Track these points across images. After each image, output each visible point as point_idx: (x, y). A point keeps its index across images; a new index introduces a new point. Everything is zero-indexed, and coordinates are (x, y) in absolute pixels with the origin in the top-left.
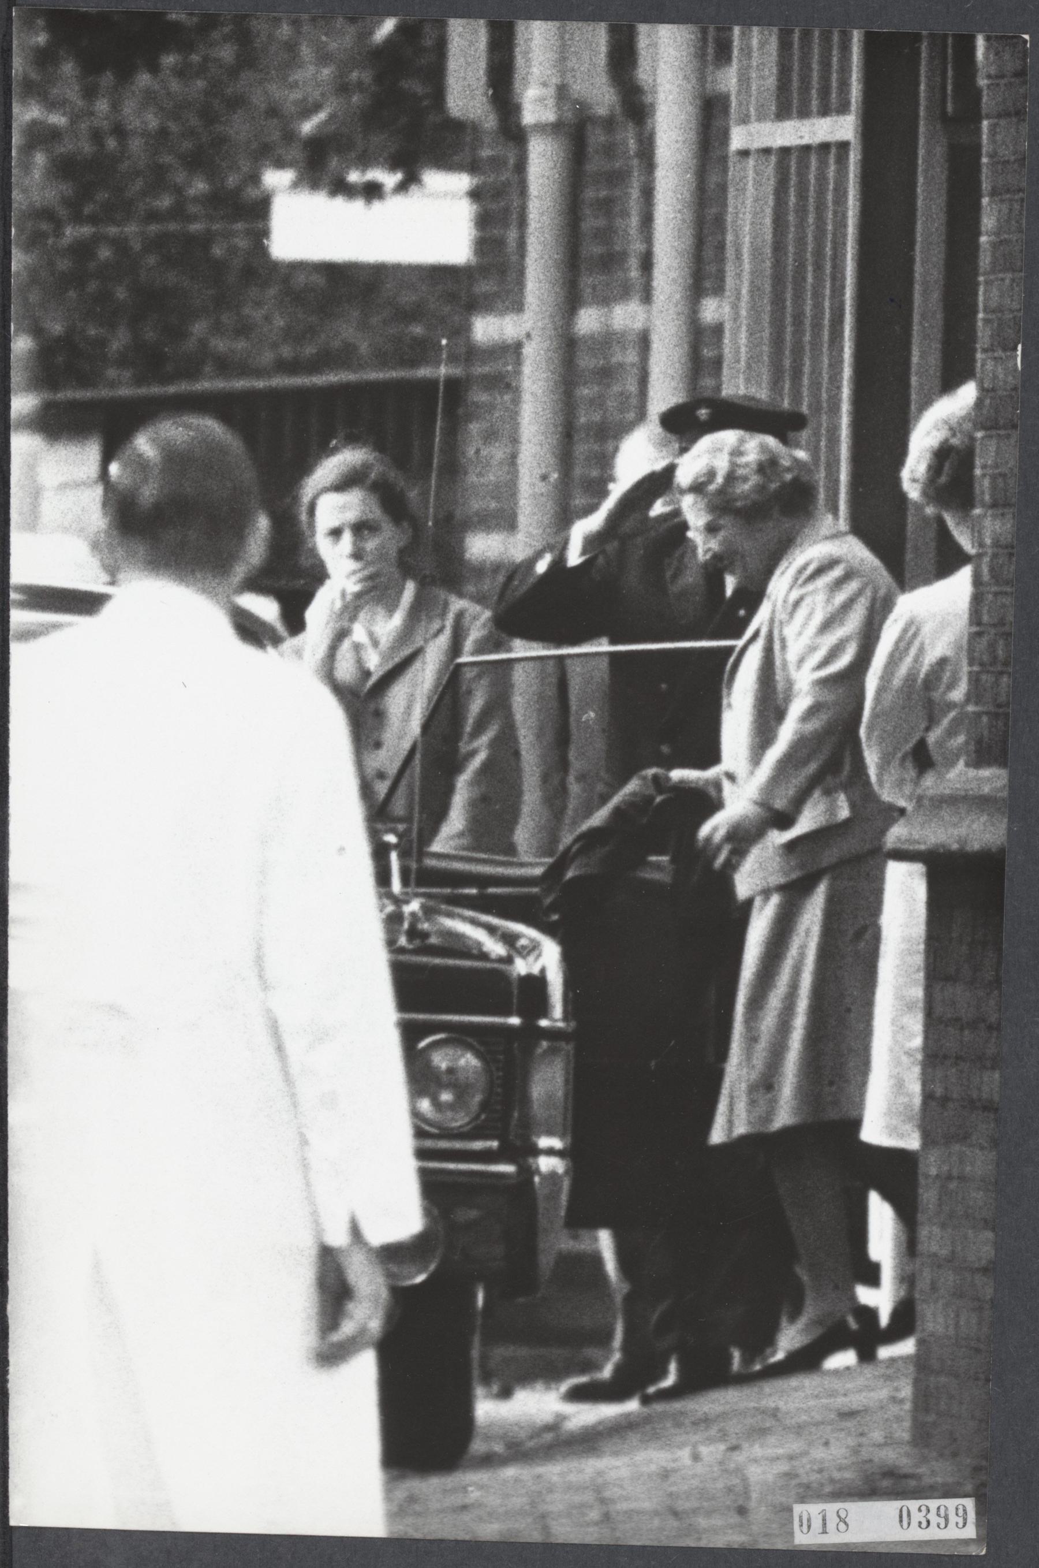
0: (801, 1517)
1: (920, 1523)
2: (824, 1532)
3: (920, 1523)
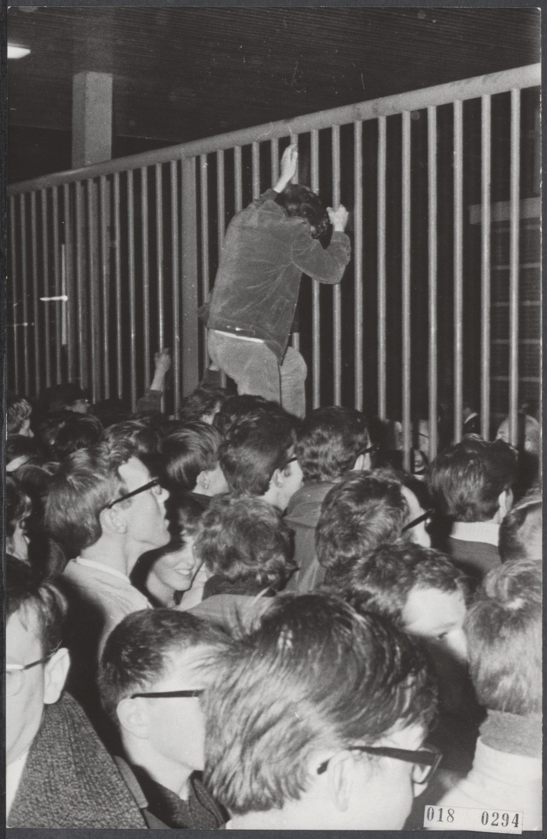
0: (429, 810)
1: (502, 824)
2: (440, 820)
3: (502, 824)
